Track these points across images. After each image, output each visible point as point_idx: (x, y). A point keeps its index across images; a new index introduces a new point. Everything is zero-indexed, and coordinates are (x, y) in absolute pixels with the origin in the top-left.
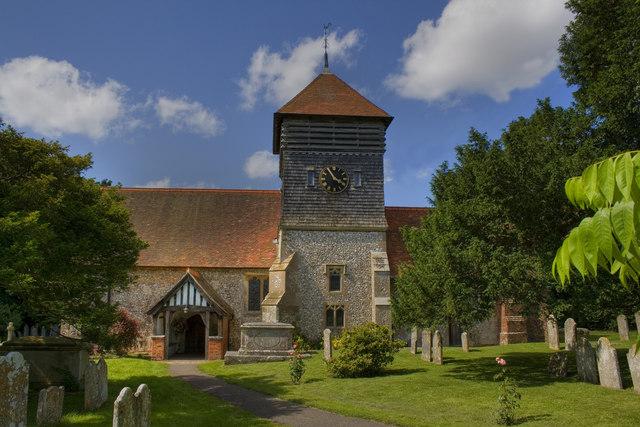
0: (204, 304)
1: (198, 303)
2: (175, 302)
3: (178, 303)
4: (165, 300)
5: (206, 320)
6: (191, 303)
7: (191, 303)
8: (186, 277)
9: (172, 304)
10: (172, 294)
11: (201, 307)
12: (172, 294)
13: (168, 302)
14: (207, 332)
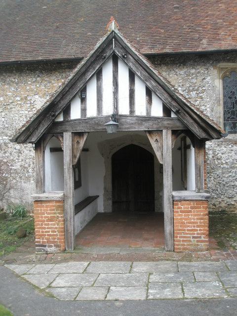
0: (157, 110)
1: (141, 109)
2: (84, 110)
3: (92, 112)
5: (164, 148)
6: (124, 109)
7: (124, 109)
8: (108, 43)
9: (75, 113)
11: (148, 118)
13: (67, 111)
14: (168, 180)
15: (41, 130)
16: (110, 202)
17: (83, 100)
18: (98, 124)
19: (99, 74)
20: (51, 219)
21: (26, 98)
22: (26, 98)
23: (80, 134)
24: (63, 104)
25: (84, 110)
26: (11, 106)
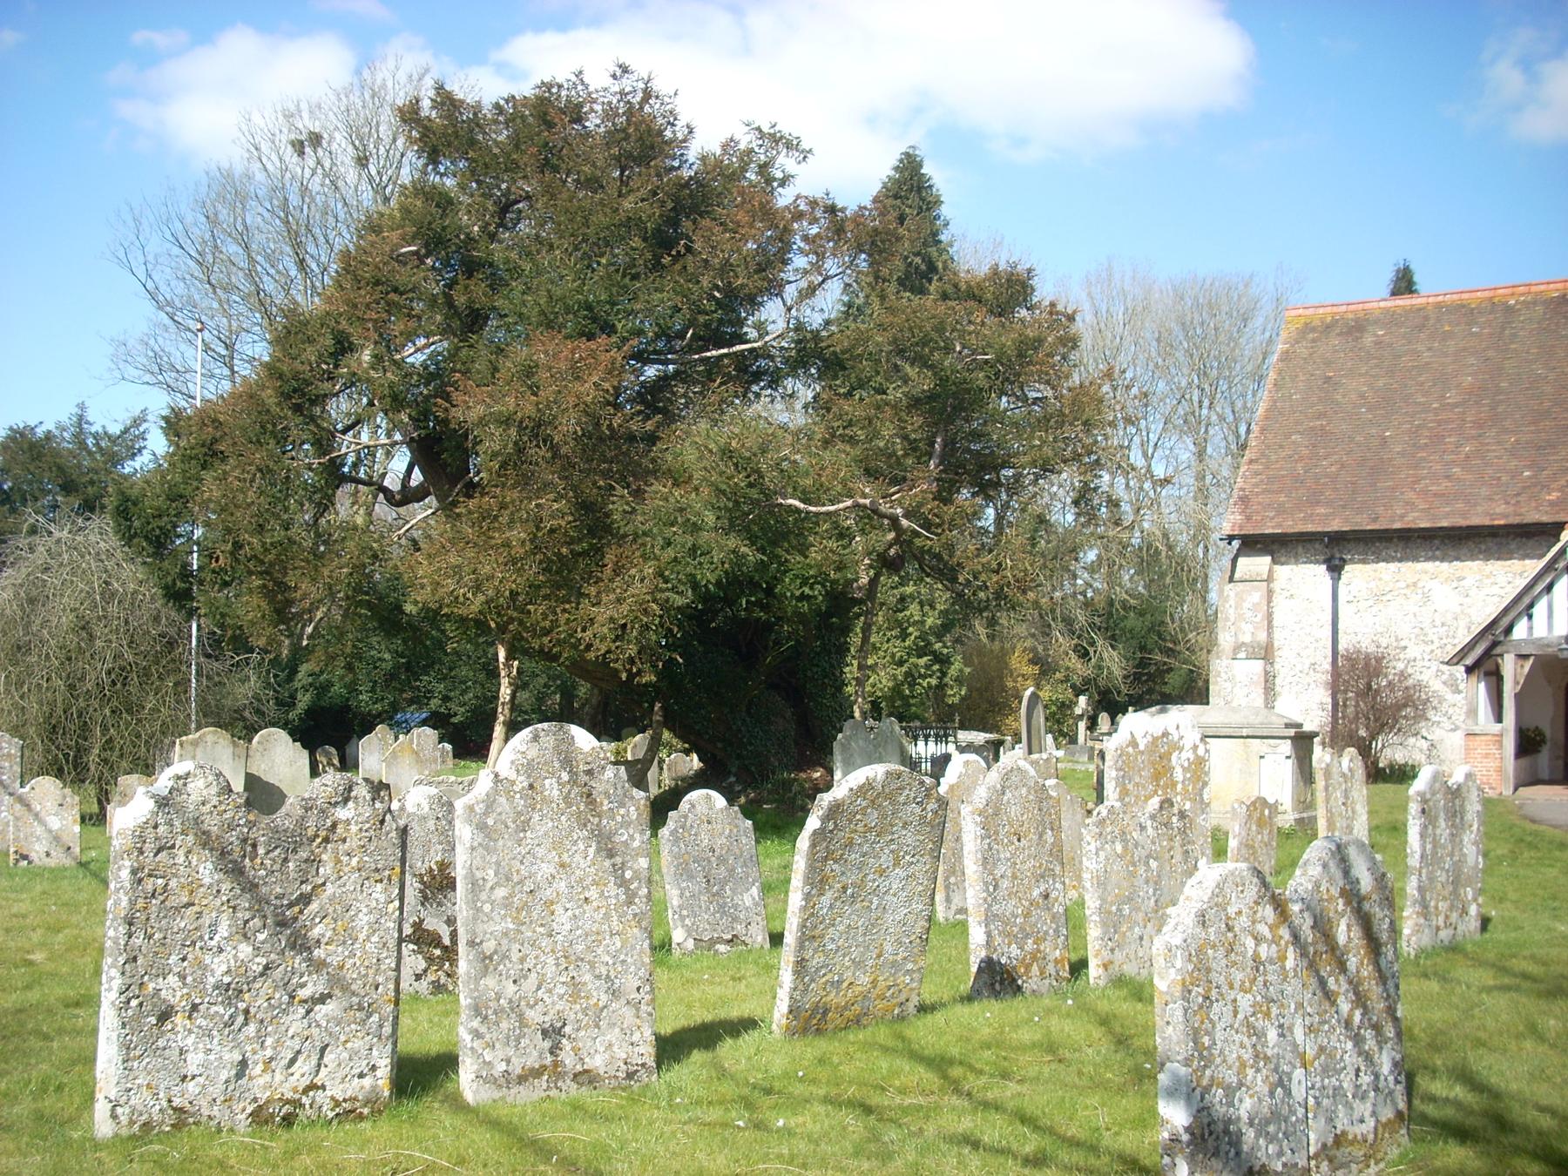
2: (1531, 628)
3: (1540, 631)
4: (1494, 636)
9: (1520, 632)
10: (1522, 605)
12: (1522, 605)
13: (1509, 630)
15: (1479, 650)
16: (1561, 763)
17: (1530, 617)
18: (1548, 646)
19: (1549, 588)
20: (1487, 756)
21: (1415, 584)
22: (1415, 584)
23: (1525, 657)
24: (1505, 622)
25: (1531, 628)
26: (1389, 597)
